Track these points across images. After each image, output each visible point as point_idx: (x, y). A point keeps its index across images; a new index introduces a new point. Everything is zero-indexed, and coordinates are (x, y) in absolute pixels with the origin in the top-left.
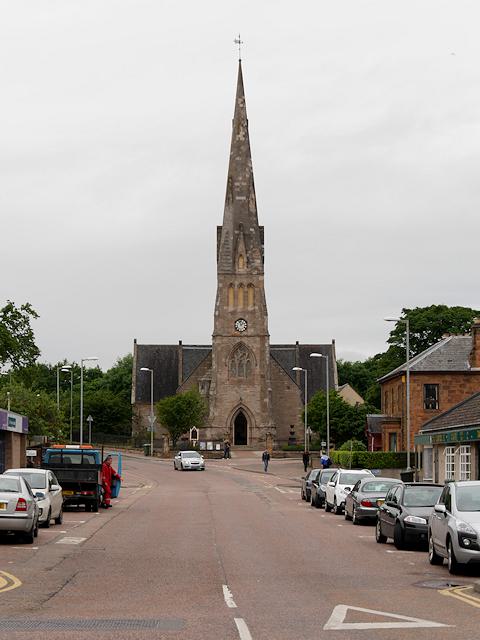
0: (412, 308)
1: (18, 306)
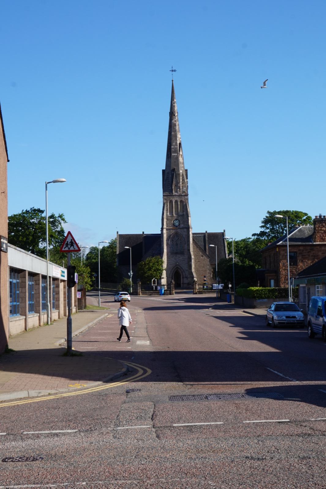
0: (272, 211)
1: (57, 215)
